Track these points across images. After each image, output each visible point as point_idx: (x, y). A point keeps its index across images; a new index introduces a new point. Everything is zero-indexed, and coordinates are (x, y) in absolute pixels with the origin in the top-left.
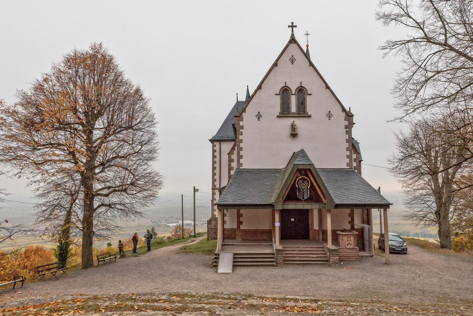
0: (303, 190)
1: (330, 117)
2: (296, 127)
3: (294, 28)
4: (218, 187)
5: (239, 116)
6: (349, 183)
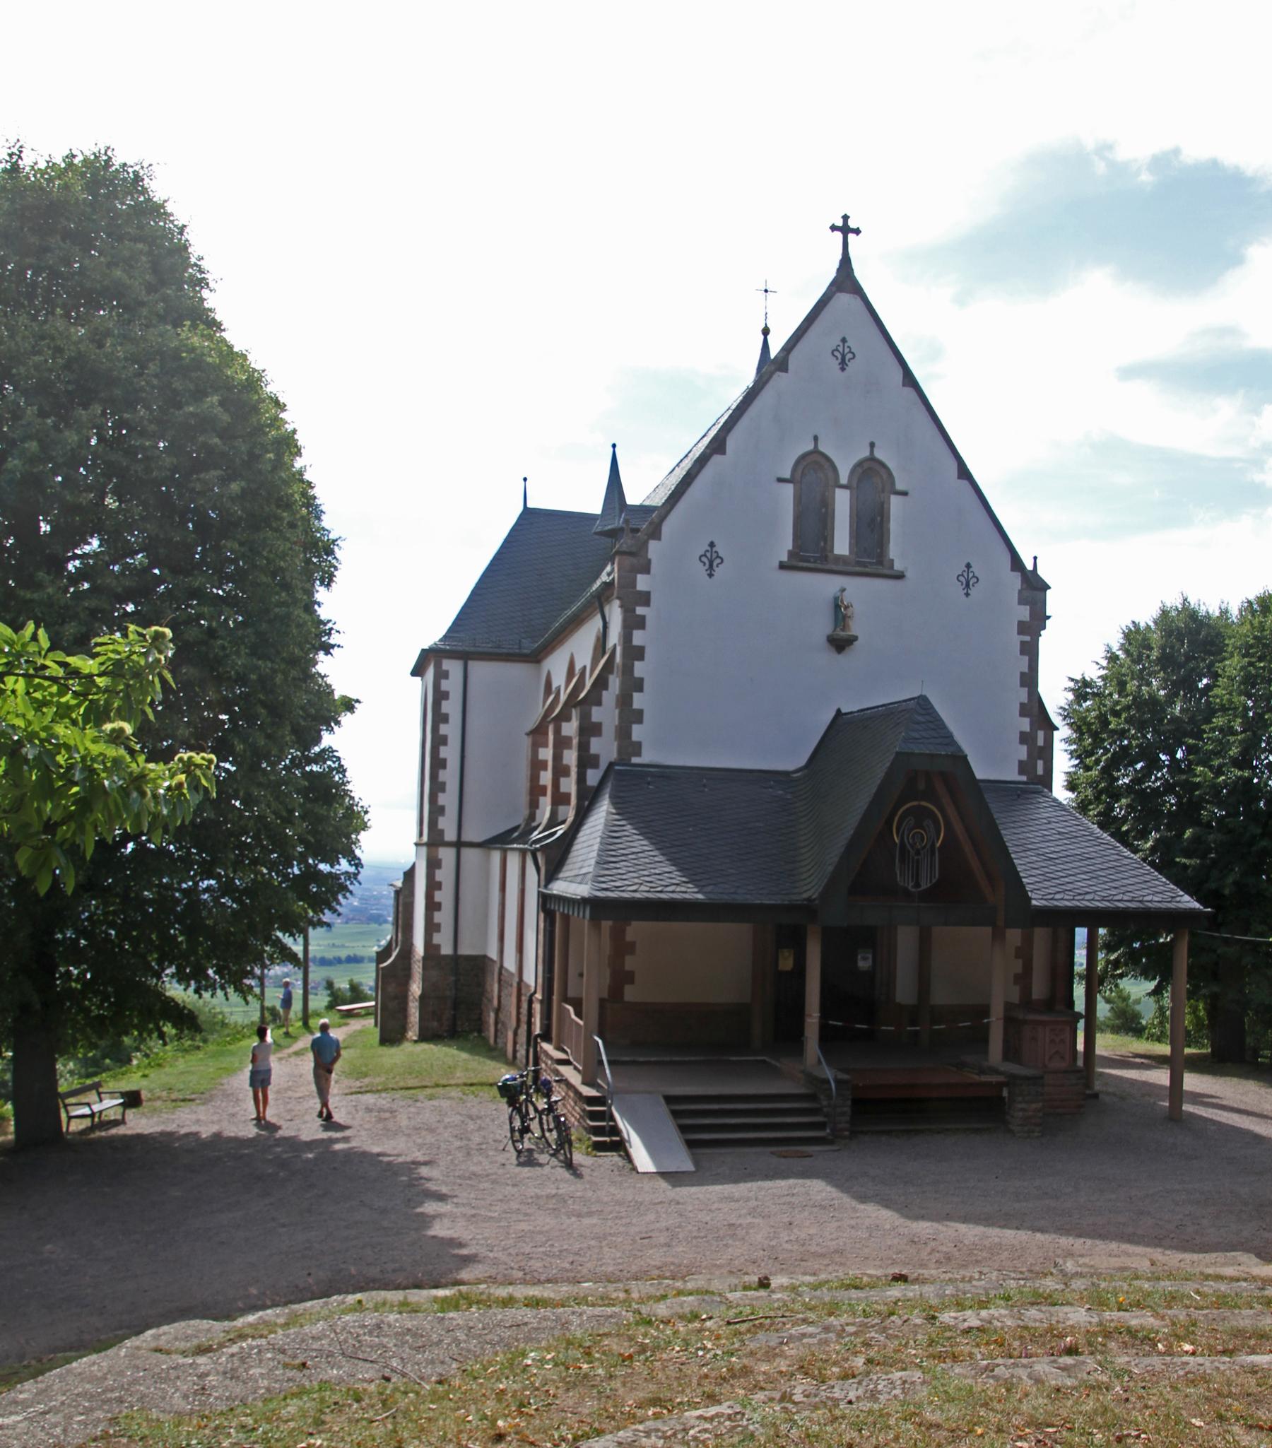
0: (918, 853)
1: (968, 585)
2: (849, 612)
3: (851, 237)
4: (450, 835)
5: (634, 549)
6: (632, 844)
